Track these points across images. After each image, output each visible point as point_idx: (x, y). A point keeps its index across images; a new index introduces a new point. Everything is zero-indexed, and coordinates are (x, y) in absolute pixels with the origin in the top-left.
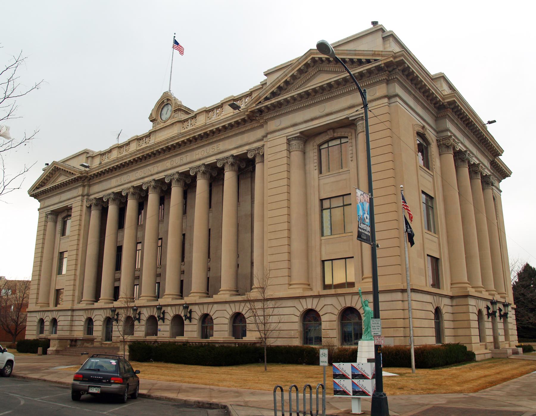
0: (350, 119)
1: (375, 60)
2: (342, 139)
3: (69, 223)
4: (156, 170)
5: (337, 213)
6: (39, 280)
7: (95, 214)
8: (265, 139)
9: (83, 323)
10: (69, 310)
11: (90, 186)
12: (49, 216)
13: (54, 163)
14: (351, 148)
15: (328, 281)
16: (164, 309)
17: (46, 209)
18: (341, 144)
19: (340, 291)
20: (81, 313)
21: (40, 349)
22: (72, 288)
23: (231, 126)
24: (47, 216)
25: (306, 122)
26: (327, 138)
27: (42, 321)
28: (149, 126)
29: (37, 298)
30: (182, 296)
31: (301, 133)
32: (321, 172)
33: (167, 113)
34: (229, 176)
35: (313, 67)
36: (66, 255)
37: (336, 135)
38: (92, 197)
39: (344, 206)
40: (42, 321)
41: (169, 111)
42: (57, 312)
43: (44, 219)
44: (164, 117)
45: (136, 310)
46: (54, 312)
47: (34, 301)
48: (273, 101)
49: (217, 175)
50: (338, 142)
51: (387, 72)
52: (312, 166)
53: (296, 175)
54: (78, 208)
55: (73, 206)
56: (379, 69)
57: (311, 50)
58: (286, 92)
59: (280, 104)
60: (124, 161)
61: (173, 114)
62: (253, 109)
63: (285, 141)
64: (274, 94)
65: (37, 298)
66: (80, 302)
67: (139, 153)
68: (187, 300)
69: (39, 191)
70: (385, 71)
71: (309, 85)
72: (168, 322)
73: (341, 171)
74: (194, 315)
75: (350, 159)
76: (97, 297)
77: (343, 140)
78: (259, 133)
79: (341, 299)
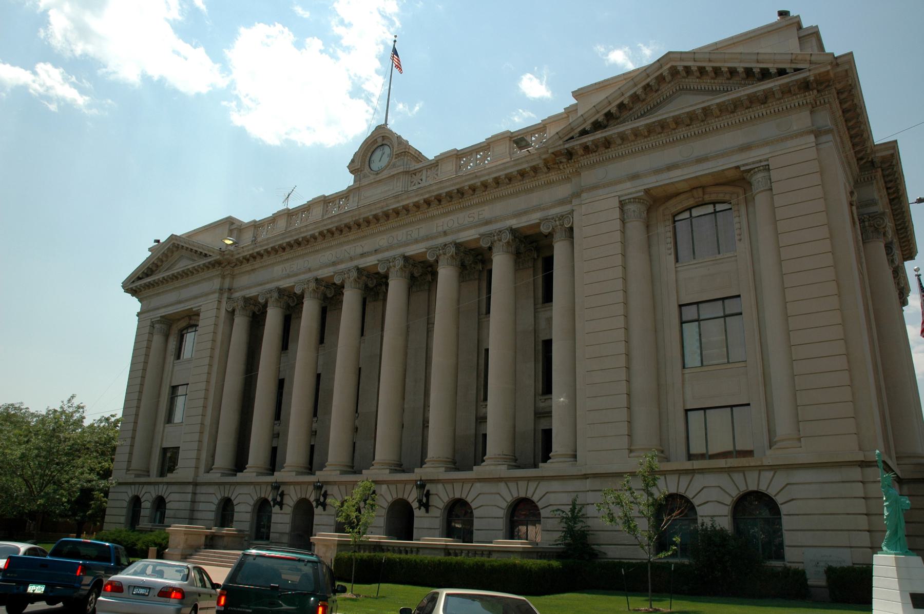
0: (742, 169)
1: (796, 70)
2: (717, 206)
3: (189, 338)
4: (359, 251)
5: (713, 329)
6: (134, 430)
7: (241, 323)
8: (575, 202)
9: (214, 507)
10: (189, 483)
11: (233, 276)
12: (157, 326)
13: (173, 237)
14: (737, 219)
15: (697, 447)
16: (428, 487)
17: (151, 313)
18: (715, 212)
19: (722, 463)
20: (211, 489)
21: (153, 550)
22: (195, 445)
23: (510, 179)
24: (152, 326)
25: (658, 171)
26: (691, 202)
27: (136, 502)
28: (347, 180)
29: (129, 462)
30: (311, 469)
31: (647, 191)
32: (677, 260)
33: (380, 160)
34: (396, 288)
35: (669, 82)
36: (181, 390)
37: (707, 198)
38: (237, 295)
39: (725, 316)
40: (136, 502)
41: (385, 156)
42: (165, 487)
43: (147, 330)
44: (376, 166)
45: (320, 488)
46: (161, 486)
47: (125, 465)
48: (599, 135)
49: (376, 286)
50: (710, 209)
51: (815, 91)
52: (664, 250)
53: (637, 262)
54: (210, 312)
55: (203, 309)
56: (806, 86)
57: (669, 53)
58: (618, 124)
59: (607, 143)
60: (303, 235)
61: (394, 160)
62: (558, 148)
63: (617, 204)
64: (597, 126)
65: (129, 462)
66: (209, 470)
67: (332, 223)
68: (278, 476)
69: (140, 284)
70: (812, 90)
71: (660, 112)
72: (288, 509)
73: (719, 257)
74: (434, 501)
75: (737, 238)
76: (240, 462)
77: (719, 207)
78: (563, 190)
79: (738, 477)
